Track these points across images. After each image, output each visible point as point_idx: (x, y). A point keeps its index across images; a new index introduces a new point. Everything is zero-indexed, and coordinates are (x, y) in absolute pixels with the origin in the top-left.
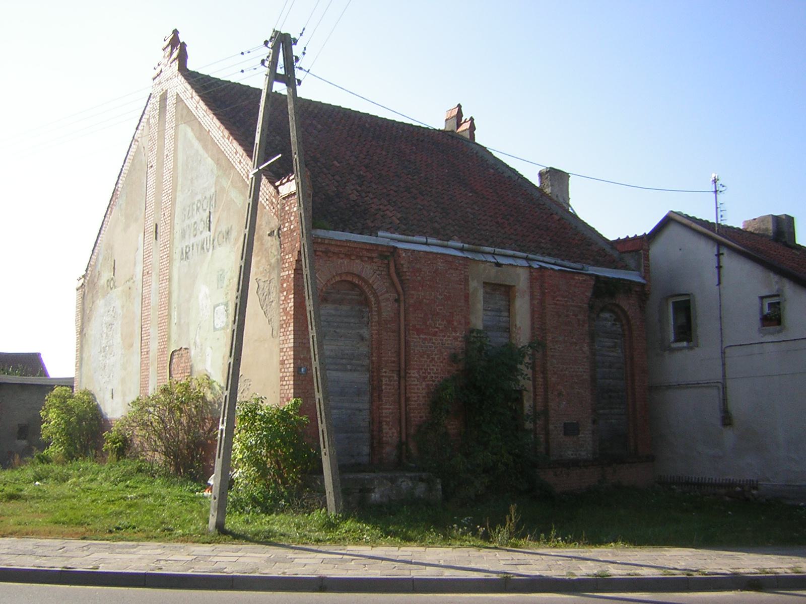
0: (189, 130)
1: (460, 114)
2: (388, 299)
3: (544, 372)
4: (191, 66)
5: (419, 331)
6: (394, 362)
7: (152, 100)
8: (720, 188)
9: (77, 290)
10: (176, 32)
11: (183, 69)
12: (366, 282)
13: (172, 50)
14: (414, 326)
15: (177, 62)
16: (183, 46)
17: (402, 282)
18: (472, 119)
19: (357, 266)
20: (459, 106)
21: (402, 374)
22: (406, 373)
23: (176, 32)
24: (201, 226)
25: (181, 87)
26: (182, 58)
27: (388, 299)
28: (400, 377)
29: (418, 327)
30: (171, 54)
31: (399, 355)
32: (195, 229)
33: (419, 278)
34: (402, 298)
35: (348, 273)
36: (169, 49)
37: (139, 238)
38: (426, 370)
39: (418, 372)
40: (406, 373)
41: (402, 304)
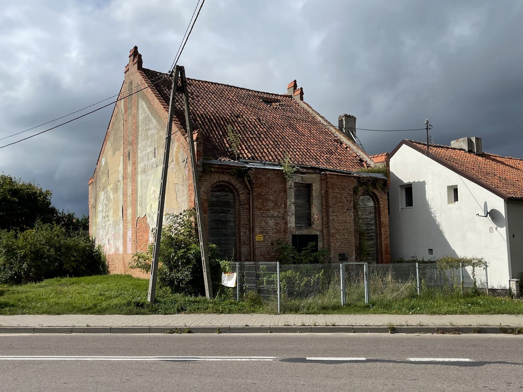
0: (144, 103)
1: (295, 86)
2: (243, 193)
3: (328, 227)
4: (144, 66)
5: (260, 209)
6: (247, 224)
7: (125, 85)
8: (430, 127)
9: (130, 57)
10: (136, 48)
11: (140, 67)
12: (232, 185)
13: (134, 58)
14: (257, 206)
15: (137, 64)
16: (140, 56)
17: (250, 184)
18: (301, 89)
19: (226, 178)
20: (295, 81)
21: (251, 230)
22: (253, 230)
23: (136, 48)
24: (151, 155)
25: (138, 78)
26: (140, 63)
27: (243, 193)
28: (250, 232)
29: (259, 207)
30: (134, 60)
31: (250, 222)
32: (148, 156)
33: (260, 182)
34: (251, 192)
35: (219, 182)
36: (132, 57)
37: (155, 106)
38: (263, 228)
39: (259, 229)
40: (253, 230)
41: (251, 195)
